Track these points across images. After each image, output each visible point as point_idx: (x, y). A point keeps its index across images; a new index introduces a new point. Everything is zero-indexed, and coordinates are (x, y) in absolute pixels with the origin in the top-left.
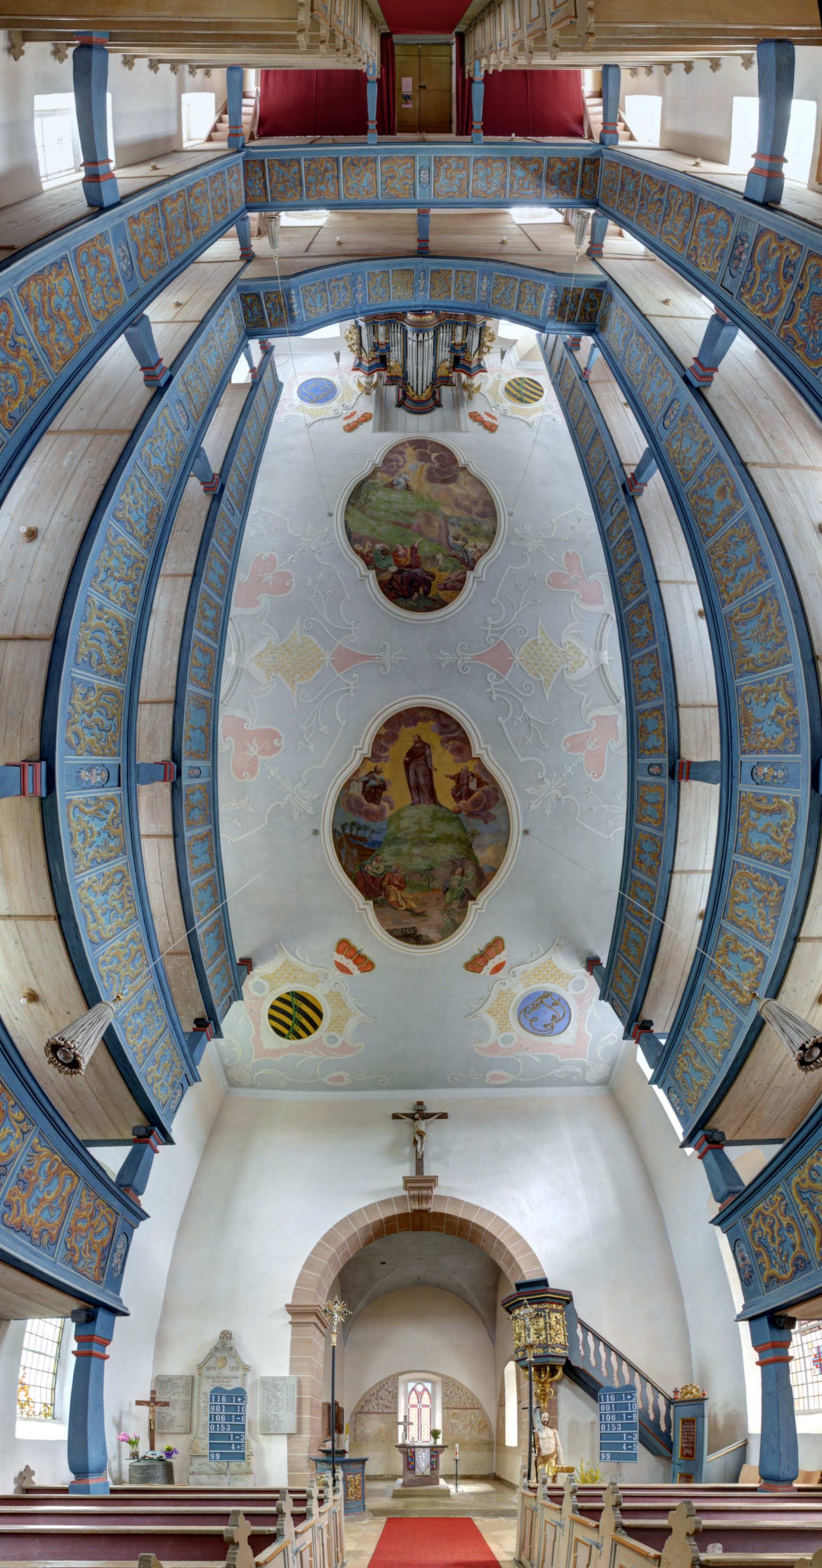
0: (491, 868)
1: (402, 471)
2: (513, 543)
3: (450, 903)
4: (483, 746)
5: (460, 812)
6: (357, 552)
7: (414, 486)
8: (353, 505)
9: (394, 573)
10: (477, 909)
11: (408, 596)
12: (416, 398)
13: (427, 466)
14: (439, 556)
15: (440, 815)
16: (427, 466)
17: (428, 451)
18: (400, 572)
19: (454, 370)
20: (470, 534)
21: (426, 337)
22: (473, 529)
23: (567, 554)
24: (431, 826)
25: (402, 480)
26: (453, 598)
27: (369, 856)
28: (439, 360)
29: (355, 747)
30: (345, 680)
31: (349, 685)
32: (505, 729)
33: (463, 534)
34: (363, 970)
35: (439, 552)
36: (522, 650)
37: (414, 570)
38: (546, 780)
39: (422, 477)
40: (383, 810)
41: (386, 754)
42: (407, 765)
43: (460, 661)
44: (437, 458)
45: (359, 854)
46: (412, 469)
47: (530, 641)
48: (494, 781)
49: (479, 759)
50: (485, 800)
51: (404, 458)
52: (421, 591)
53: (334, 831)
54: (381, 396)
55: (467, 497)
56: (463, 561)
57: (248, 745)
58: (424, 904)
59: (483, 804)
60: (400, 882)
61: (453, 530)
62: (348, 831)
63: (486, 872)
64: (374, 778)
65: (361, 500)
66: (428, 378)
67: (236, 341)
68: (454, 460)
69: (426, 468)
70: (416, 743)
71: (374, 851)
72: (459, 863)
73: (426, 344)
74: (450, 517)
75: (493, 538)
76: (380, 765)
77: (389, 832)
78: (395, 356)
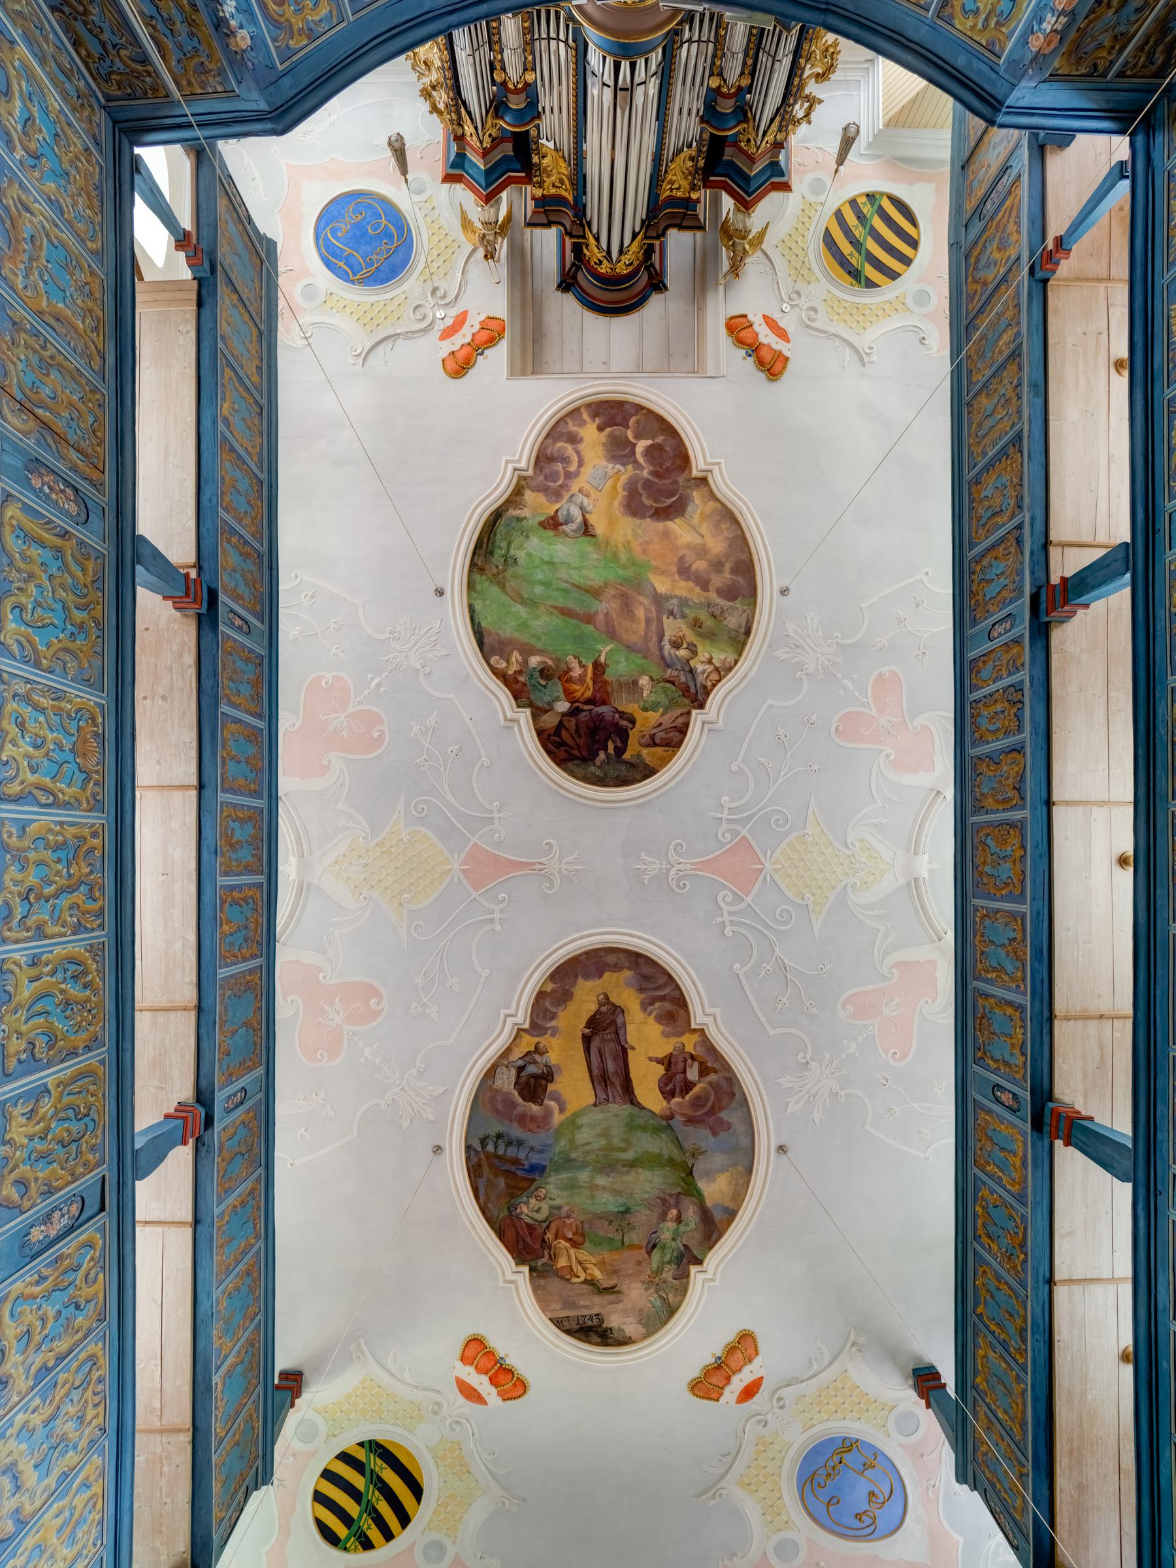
0: (726, 1209)
1: (575, 487)
2: (781, 653)
3: (660, 1271)
4: (708, 1011)
5: (672, 1117)
6: (494, 671)
7: (599, 526)
8: (482, 570)
9: (564, 715)
10: (705, 1280)
11: (588, 758)
12: (604, 269)
13: (628, 472)
14: (644, 681)
15: (640, 1121)
16: (628, 472)
17: (630, 434)
18: (574, 712)
19: (707, 184)
20: (703, 636)
21: (640, 75)
22: (709, 623)
23: (881, 675)
24: (626, 1141)
25: (575, 512)
26: (664, 761)
27: (524, 1189)
28: (672, 143)
29: (503, 1012)
30: (487, 904)
31: (493, 912)
32: (744, 983)
33: (690, 636)
34: (506, 1397)
35: (643, 672)
36: (777, 853)
37: (600, 709)
38: (813, 1064)
39: (616, 503)
40: (548, 1114)
41: (554, 1023)
42: (587, 1040)
43: (673, 872)
44: (648, 452)
45: (507, 1185)
46: (598, 479)
47: (792, 836)
48: (727, 1067)
49: (703, 1030)
50: (712, 1098)
51: (578, 453)
52: (611, 750)
53: (468, 1148)
54: (522, 251)
55: (702, 552)
56: (685, 691)
57: (326, 1007)
58: (615, 1272)
59: (710, 1104)
60: (575, 1234)
61: (672, 627)
62: (490, 1148)
63: (718, 1216)
64: (535, 1062)
65: (497, 558)
66: (637, 209)
67: (96, 167)
68: (683, 459)
69: (624, 478)
70: (601, 1005)
71: (534, 1180)
72: (672, 1201)
73: (639, 92)
74: (668, 598)
75: (744, 644)
76: (543, 1041)
77: (558, 1149)
78: (553, 130)
